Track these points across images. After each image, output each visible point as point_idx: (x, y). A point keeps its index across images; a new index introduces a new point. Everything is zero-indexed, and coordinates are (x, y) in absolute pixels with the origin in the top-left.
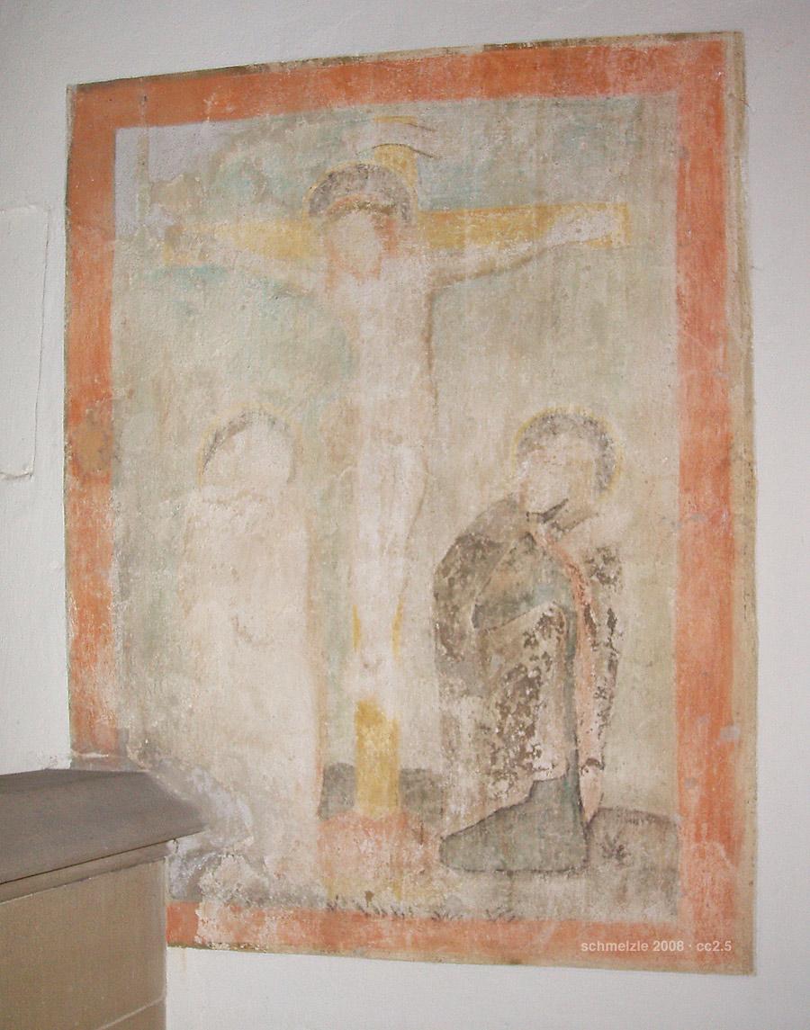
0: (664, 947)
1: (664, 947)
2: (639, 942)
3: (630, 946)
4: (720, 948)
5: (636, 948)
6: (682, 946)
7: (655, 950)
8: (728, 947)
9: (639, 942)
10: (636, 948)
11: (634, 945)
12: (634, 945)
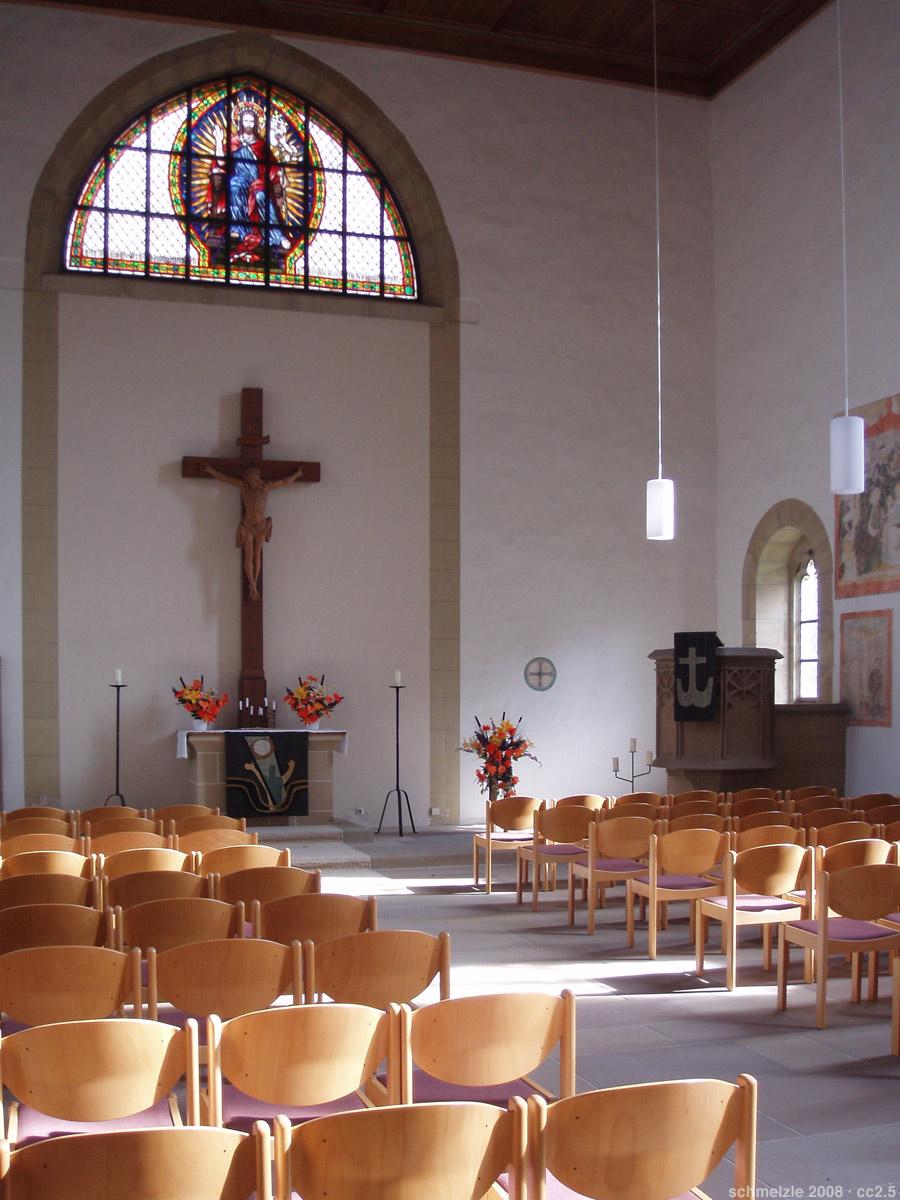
5: (790, 1193)
8: (892, 1194)
9: (780, 1188)
10: (790, 1193)
11: (788, 1190)
12: (788, 1190)
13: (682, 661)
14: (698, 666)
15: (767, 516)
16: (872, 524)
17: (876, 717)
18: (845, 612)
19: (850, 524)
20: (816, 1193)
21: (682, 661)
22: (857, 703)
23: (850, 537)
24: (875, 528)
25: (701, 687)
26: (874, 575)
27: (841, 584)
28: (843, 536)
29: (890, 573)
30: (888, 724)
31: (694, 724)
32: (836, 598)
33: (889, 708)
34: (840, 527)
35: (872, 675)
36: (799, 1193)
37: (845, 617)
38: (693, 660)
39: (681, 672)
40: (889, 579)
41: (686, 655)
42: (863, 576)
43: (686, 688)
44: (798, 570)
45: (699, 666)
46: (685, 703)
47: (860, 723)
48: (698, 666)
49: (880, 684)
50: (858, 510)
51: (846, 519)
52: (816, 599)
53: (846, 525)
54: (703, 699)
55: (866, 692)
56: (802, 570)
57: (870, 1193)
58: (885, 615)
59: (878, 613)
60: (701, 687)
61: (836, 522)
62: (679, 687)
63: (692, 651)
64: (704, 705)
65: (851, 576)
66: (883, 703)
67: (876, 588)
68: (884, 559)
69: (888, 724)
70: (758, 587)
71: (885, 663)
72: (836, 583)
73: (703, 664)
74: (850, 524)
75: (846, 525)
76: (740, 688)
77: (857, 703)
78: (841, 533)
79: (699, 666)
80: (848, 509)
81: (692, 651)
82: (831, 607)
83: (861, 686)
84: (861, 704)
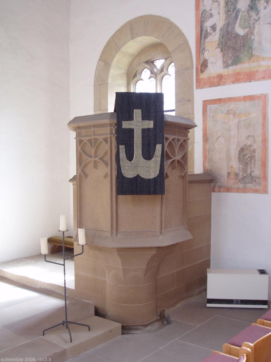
0: (29, 359)
1: (29, 359)
2: (16, 358)
3: (17, 360)
4: (47, 360)
6: (34, 359)
7: (26, 361)
8: (50, 360)
9: (16, 358)
10: (19, 360)
11: (19, 359)
12: (19, 359)
13: (126, 125)
14: (144, 131)
15: (121, 31)
16: (240, 26)
17: (247, 185)
18: (204, 100)
19: (214, 28)
20: (27, 360)
21: (126, 125)
22: (224, 172)
23: (215, 38)
24: (243, 28)
25: (148, 155)
26: (245, 66)
27: (202, 76)
28: (206, 37)
29: (263, 63)
30: (265, 191)
31: (129, 197)
32: (197, 88)
33: (265, 177)
34: (201, 31)
35: (242, 150)
36: (22, 360)
37: (206, 103)
38: (138, 124)
39: (124, 138)
40: (262, 69)
41: (130, 118)
42: (231, 68)
43: (130, 157)
44: (135, 76)
45: (145, 132)
46: (129, 173)
47: (228, 190)
48: (144, 131)
49: (252, 157)
50: (223, 16)
51: (208, 24)
52: (175, 88)
53: (209, 29)
54: (149, 170)
55: (235, 165)
56: (138, 76)
57: (5, 360)
58: (264, 98)
59: (251, 98)
60: (148, 155)
61: (196, 26)
62: (123, 155)
63: (137, 113)
64: (152, 177)
65: (216, 66)
66: (257, 172)
67: (250, 77)
68: (254, 52)
69: (265, 191)
70: (109, 85)
71: (259, 139)
72: (197, 75)
73: (149, 129)
74: (214, 28)
75: (209, 29)
76: (174, 158)
77: (224, 172)
78: (202, 35)
79: (145, 132)
80: (211, 15)
81: (137, 113)
82: (192, 95)
83: (229, 159)
84: (229, 174)
